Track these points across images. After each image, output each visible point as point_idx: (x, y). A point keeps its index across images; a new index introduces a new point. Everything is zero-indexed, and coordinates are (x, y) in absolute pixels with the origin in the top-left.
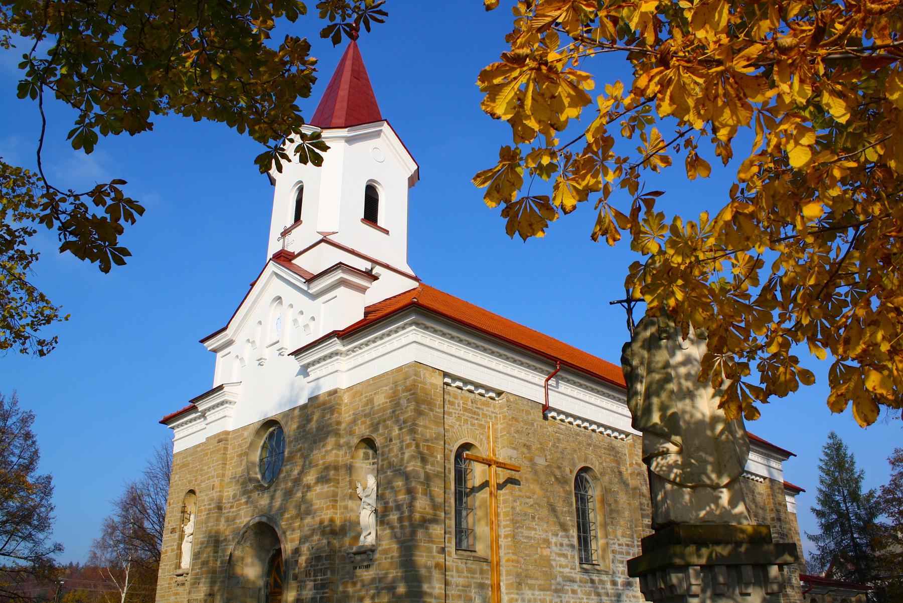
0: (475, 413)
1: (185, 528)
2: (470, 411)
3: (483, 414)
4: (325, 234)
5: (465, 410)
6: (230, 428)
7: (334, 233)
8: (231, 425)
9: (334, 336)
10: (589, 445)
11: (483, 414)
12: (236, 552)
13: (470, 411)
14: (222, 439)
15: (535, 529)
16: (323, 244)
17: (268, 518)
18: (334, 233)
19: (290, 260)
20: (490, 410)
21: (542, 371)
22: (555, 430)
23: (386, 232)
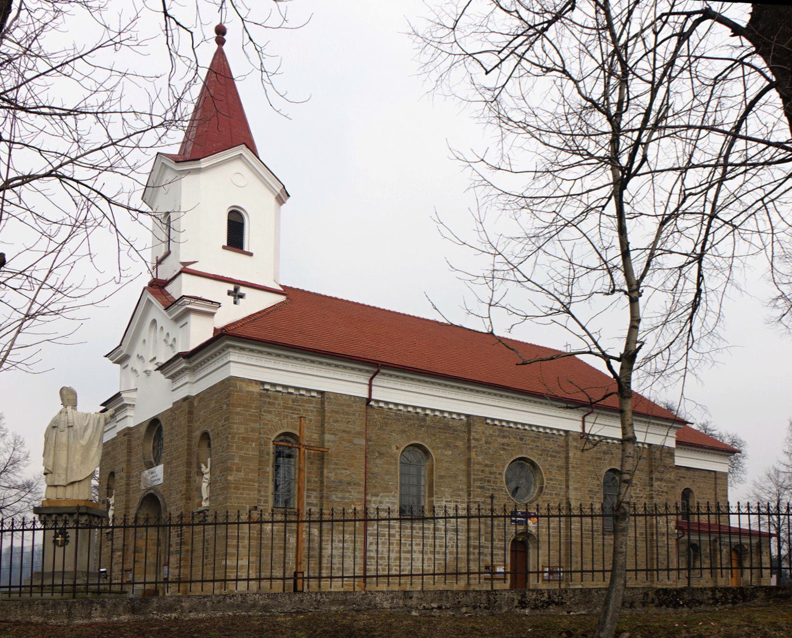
0: (295, 409)
1: (110, 499)
2: (291, 408)
3: (304, 410)
4: (185, 264)
5: (286, 408)
6: (132, 425)
7: (194, 262)
8: (131, 423)
9: (179, 357)
10: (422, 426)
11: (304, 410)
12: (270, 527)
13: (291, 408)
14: (128, 432)
15: (350, 492)
16: (183, 275)
17: (155, 491)
18: (194, 262)
19: (163, 287)
20: (312, 405)
21: (368, 371)
22: (383, 416)
23: (251, 254)
